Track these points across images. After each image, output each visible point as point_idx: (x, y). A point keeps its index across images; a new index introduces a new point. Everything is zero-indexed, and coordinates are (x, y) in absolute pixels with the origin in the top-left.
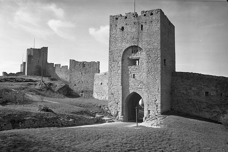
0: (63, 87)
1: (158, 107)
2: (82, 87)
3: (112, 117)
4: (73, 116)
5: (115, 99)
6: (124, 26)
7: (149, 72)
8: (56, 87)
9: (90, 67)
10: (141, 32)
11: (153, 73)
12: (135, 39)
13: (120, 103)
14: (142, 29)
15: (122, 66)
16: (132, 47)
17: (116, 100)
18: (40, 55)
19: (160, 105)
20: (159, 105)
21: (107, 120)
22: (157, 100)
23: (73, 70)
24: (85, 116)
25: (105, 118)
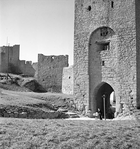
0: (30, 81)
1: (133, 100)
2: (50, 83)
3: (78, 112)
4: (28, 108)
5: (81, 91)
6: (91, 5)
7: (121, 57)
8: (23, 81)
9: (59, 61)
10: (111, 10)
11: (126, 58)
12: (104, 19)
13: (87, 95)
14: (112, 7)
15: (89, 52)
16: (101, 28)
17: (82, 92)
18: (12, 53)
19: (136, 97)
20: (135, 97)
21: (71, 115)
22: (131, 91)
23: (41, 64)
24: (44, 109)
25: (69, 113)
